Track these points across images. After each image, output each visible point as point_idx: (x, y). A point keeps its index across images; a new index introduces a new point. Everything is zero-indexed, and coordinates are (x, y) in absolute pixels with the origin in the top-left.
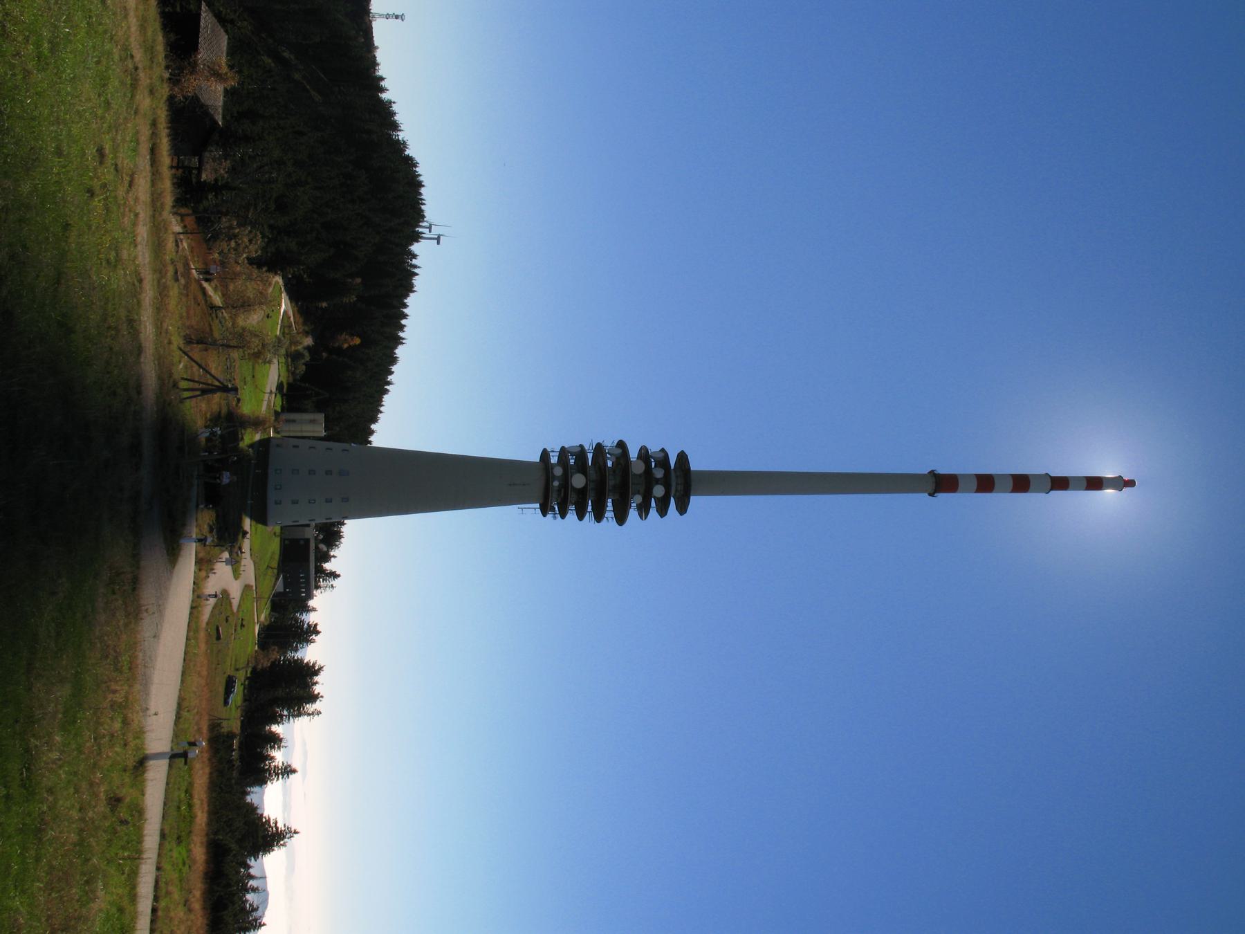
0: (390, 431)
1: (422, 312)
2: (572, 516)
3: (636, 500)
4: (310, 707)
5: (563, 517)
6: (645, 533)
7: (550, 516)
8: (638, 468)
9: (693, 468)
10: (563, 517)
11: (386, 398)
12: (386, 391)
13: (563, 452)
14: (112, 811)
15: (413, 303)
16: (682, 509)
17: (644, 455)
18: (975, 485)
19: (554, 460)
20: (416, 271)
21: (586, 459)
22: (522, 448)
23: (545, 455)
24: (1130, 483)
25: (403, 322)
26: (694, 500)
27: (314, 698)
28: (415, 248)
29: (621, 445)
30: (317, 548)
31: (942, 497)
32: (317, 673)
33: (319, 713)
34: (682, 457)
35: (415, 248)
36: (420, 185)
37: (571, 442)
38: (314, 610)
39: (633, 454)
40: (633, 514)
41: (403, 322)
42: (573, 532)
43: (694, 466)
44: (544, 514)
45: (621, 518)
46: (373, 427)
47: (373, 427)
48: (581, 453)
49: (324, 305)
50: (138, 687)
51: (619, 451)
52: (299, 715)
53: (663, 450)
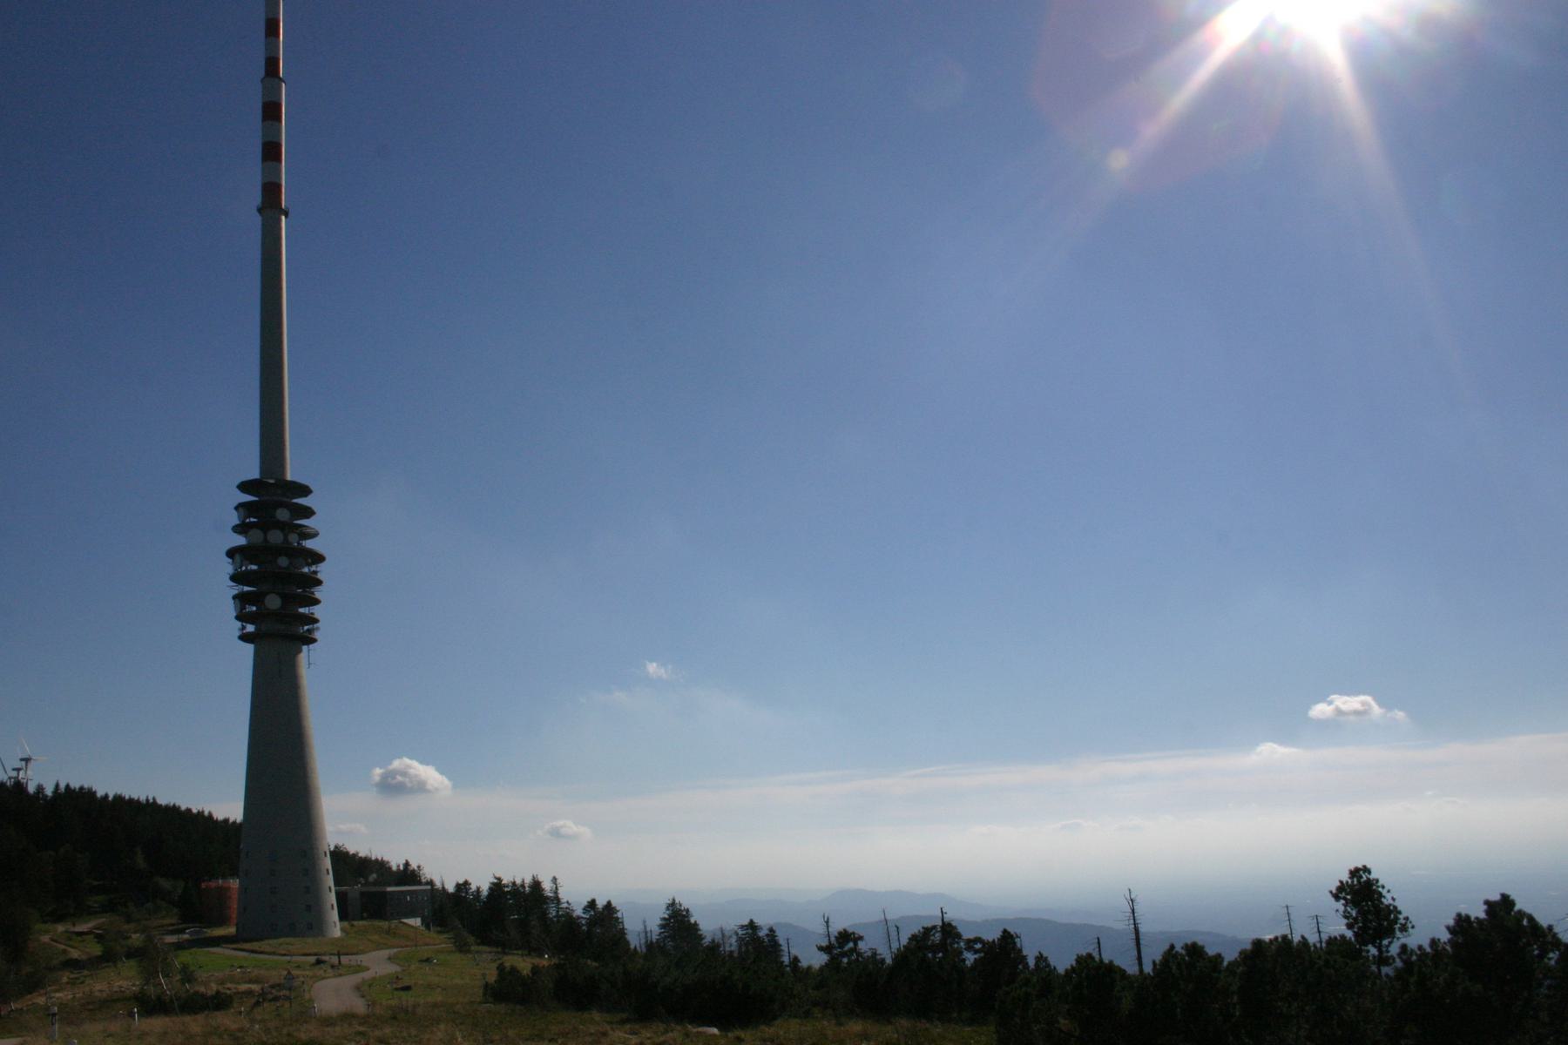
0: (229, 806)
1: (113, 779)
2: (317, 611)
3: (293, 538)
4: (547, 886)
5: (316, 621)
6: (337, 530)
8: (257, 536)
10: (316, 621)
15: (105, 787)
16: (305, 491)
17: (240, 529)
19: (250, 628)
21: (248, 593)
22: (237, 663)
23: (245, 638)
27: (536, 885)
29: (231, 553)
33: (555, 880)
34: (245, 487)
37: (230, 609)
39: (240, 541)
40: (309, 544)
42: (334, 606)
43: (254, 474)
44: (314, 641)
45: (318, 558)
48: (241, 599)
51: (238, 557)
52: (557, 900)
53: (236, 508)
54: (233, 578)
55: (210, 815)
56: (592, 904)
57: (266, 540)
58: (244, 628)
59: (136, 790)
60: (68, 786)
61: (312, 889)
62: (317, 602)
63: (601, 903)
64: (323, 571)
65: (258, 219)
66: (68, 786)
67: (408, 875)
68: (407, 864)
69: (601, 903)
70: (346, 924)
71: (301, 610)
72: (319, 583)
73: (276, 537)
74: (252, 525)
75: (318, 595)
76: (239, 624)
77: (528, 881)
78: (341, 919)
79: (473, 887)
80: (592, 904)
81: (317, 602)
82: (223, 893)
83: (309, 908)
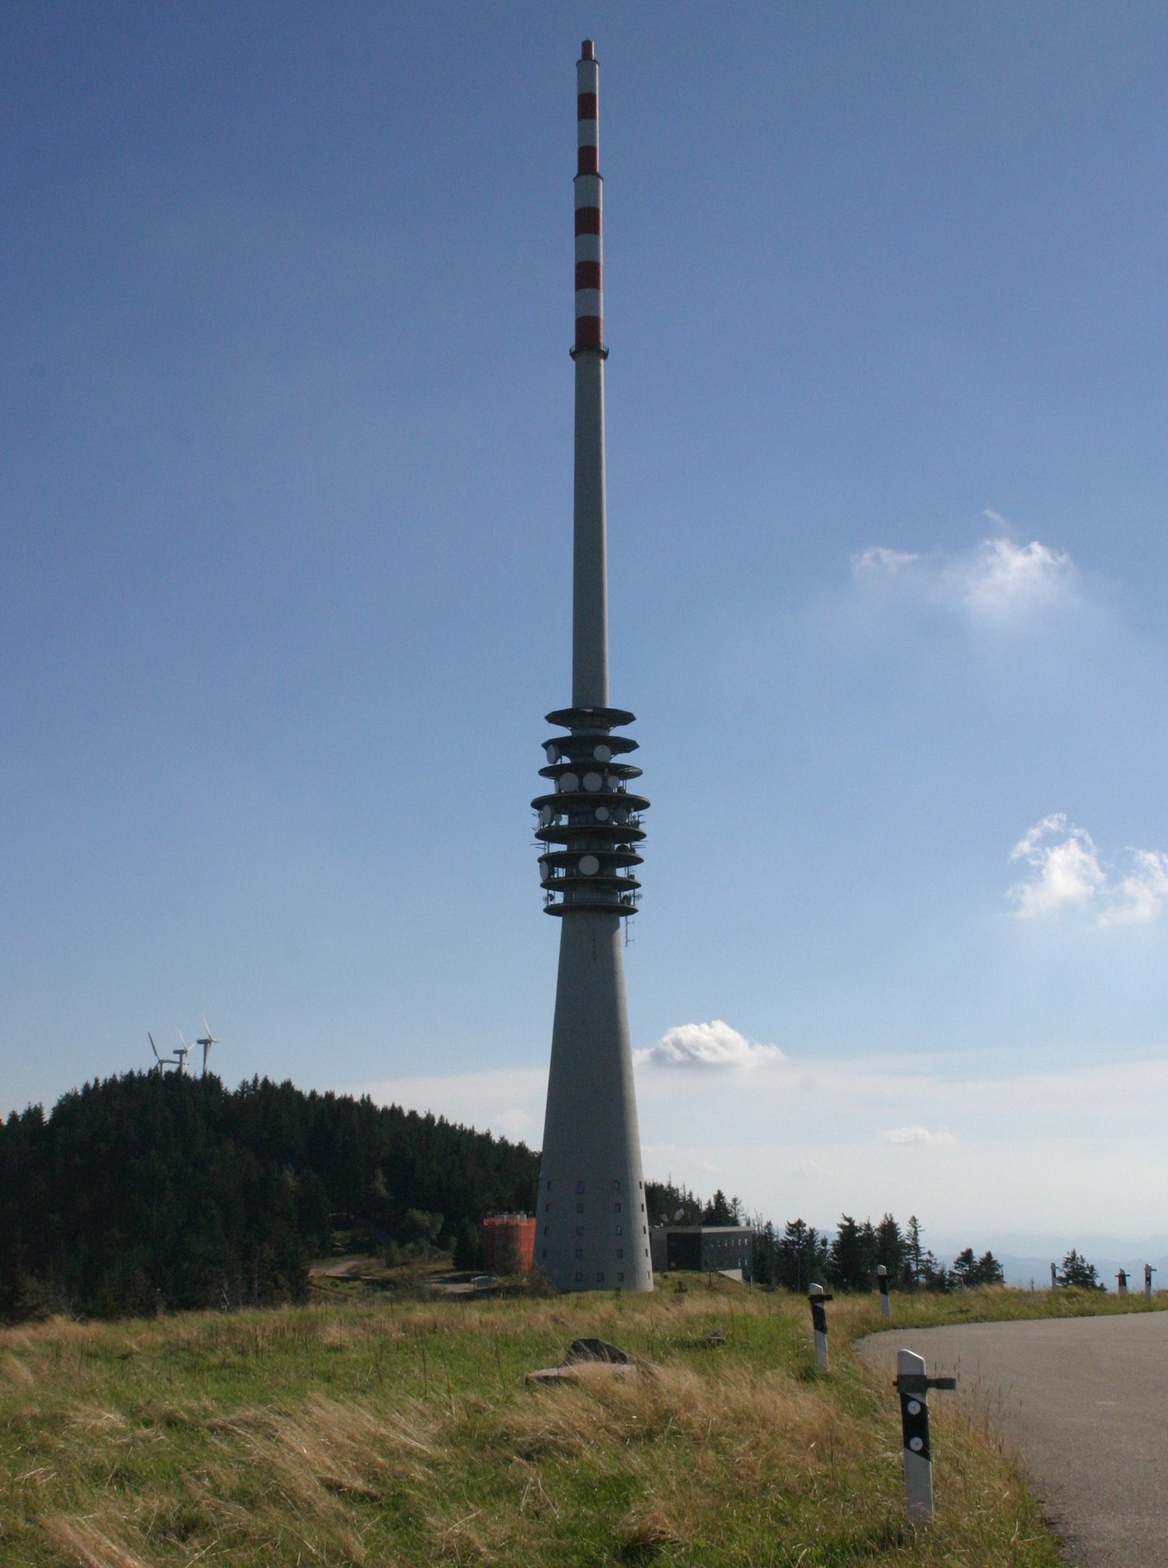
1: (324, 1069)
2: (638, 871)
4: (904, 1229)
6: (657, 771)
8: (571, 782)
9: (570, 706)
13: (549, 884)
16: (625, 718)
18: (584, 259)
19: (559, 898)
23: (551, 910)
24: (587, 46)
26: (610, 703)
27: (889, 1228)
28: (231, 1085)
29: (538, 804)
30: (679, 1223)
31: (605, 341)
33: (914, 1220)
34: (556, 718)
35: (231, 1085)
43: (567, 703)
44: (633, 911)
46: (406, 1113)
47: (406, 1113)
48: (550, 861)
50: (705, 1292)
52: (917, 1248)
53: (546, 745)
54: (540, 835)
55: (287, 1086)
56: (967, 1256)
57: (581, 787)
58: (552, 897)
59: (348, 1086)
60: (266, 1081)
61: (625, 1231)
62: (639, 861)
63: (978, 1255)
64: (646, 820)
65: (571, 364)
66: (266, 1081)
67: (721, 1212)
68: (719, 1197)
69: (978, 1255)
70: (658, 1274)
71: (563, 848)
72: (641, 836)
73: (593, 782)
74: (563, 769)
75: (639, 852)
76: (544, 892)
77: (876, 1224)
78: (655, 1269)
79: (820, 1238)
80: (967, 1256)
81: (639, 861)
82: (508, 1233)
83: (620, 1253)
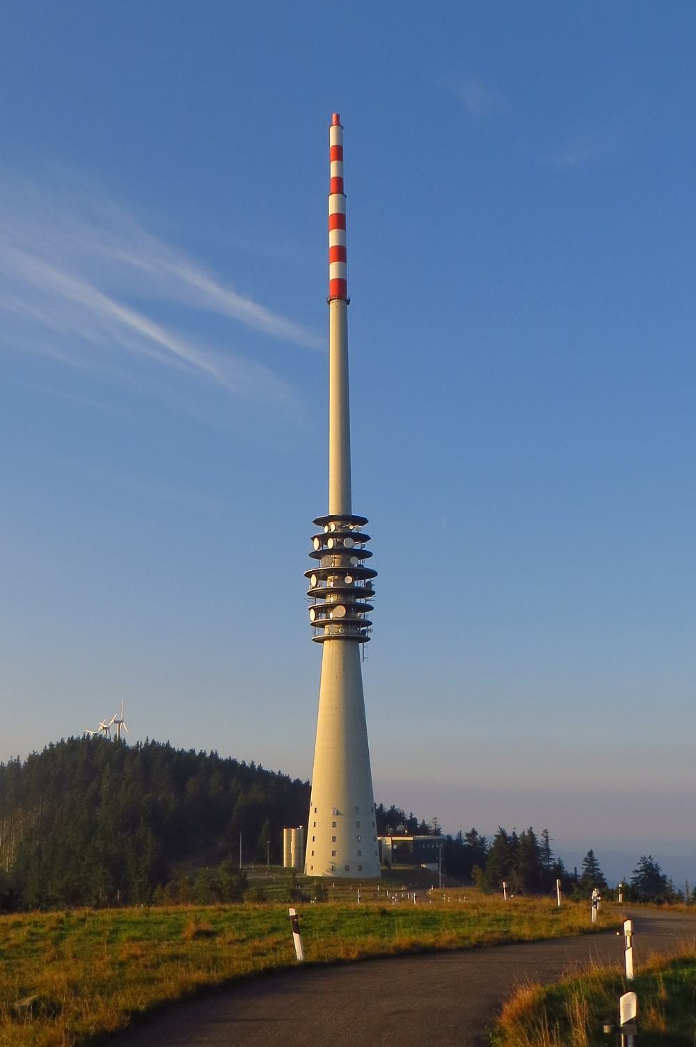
7: (369, 635)
11: (265, 768)
12: (260, 768)
14: (126, 964)
15: (181, 743)
20: (150, 742)
25: (197, 753)
32: (503, 833)
36: (71, 740)
38: (244, 762)
41: (197, 753)
42: (380, 615)
49: (424, 866)
